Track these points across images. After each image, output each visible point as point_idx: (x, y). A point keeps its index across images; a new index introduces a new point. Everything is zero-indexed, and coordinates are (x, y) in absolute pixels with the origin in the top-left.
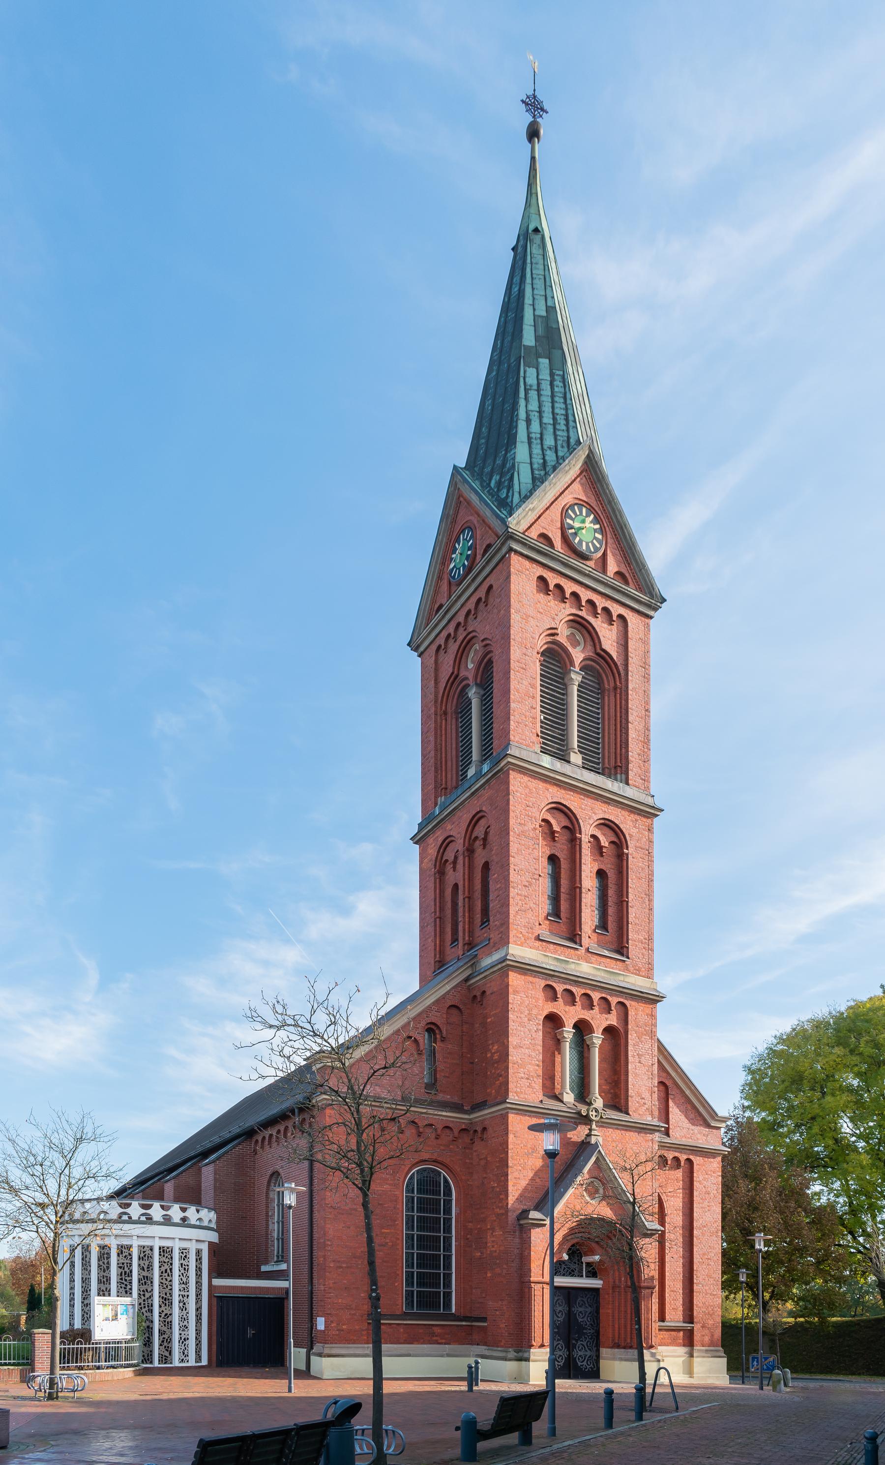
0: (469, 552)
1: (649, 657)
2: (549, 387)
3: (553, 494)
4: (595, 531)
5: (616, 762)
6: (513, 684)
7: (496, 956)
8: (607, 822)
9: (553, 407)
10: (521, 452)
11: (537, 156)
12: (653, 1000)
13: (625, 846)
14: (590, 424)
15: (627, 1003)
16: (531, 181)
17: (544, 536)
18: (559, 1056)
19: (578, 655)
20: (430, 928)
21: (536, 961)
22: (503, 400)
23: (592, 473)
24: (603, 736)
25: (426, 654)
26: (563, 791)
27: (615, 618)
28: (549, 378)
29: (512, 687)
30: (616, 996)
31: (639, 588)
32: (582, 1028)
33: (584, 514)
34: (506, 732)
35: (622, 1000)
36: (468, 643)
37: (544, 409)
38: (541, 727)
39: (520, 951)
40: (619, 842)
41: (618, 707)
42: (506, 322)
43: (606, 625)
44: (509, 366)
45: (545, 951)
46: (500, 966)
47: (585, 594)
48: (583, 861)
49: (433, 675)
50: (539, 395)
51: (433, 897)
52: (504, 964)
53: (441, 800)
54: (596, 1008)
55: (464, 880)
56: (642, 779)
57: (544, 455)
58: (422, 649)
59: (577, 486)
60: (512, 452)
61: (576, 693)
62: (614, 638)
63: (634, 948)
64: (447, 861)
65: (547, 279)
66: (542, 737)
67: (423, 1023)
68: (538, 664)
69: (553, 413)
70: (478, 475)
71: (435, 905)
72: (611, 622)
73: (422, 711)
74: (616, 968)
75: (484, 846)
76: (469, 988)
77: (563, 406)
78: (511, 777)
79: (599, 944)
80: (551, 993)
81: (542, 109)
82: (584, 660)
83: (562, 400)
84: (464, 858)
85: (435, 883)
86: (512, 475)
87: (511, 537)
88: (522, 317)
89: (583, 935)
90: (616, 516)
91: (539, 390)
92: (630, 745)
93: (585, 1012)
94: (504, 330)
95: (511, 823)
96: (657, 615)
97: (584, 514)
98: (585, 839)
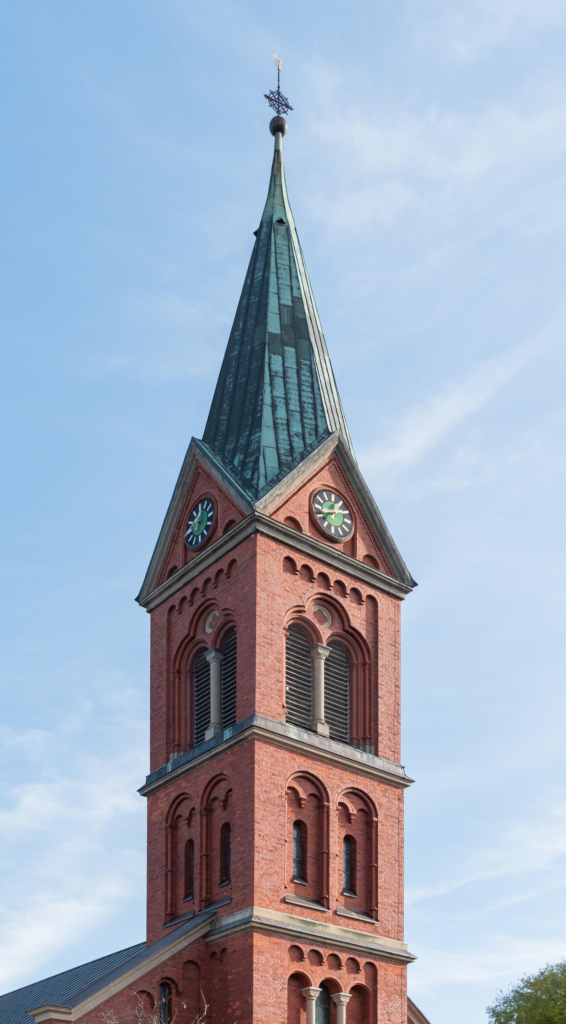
0: (209, 523)
1: (399, 636)
2: (295, 375)
3: (301, 481)
4: (344, 516)
5: (364, 734)
6: (259, 659)
7: (239, 916)
8: (356, 791)
9: (300, 395)
10: (267, 436)
11: (281, 150)
12: (403, 961)
13: (374, 815)
14: (339, 412)
15: (376, 963)
16: (275, 172)
17: (291, 520)
18: (305, 1014)
19: (326, 632)
20: (161, 881)
21: (282, 923)
22: (247, 381)
23: (342, 463)
24: (351, 708)
25: (157, 612)
26: (310, 761)
27: (364, 599)
28: (295, 367)
29: (257, 661)
30: (366, 957)
31: (390, 572)
32: (329, 987)
33: (333, 499)
34: (252, 704)
35: (371, 961)
36: (204, 610)
37: (290, 396)
38: (287, 698)
39: (264, 913)
40: (368, 809)
41: (367, 681)
42: (248, 304)
43: (355, 605)
44: (252, 349)
45: (291, 913)
46: (243, 927)
47: (333, 576)
48: (331, 828)
49: (165, 633)
50: (285, 383)
51: (164, 850)
52: (248, 925)
53: (174, 756)
54: (344, 969)
55: (201, 838)
56: (392, 751)
57: (291, 442)
58: (152, 606)
59: (325, 474)
60: (257, 435)
61: (323, 666)
62: (364, 616)
63: (383, 912)
64: (180, 816)
65: (293, 270)
66: (288, 708)
67: (158, 978)
68: (284, 638)
69: (300, 401)
70: (219, 450)
71: (167, 858)
72: (359, 600)
73: (151, 667)
74: (364, 930)
75: (225, 807)
76: (207, 944)
77: (311, 395)
78: (256, 746)
79: (347, 906)
80: (297, 953)
81: (287, 106)
82: (332, 636)
83: (309, 389)
84: (202, 817)
85: (167, 836)
86: (258, 458)
87: (258, 520)
88: (266, 305)
89: (331, 898)
90: (366, 504)
91: (284, 377)
92: (380, 719)
93: (333, 971)
94: (247, 312)
95: (256, 790)
96: (407, 597)
97: (333, 499)
98: (333, 807)
